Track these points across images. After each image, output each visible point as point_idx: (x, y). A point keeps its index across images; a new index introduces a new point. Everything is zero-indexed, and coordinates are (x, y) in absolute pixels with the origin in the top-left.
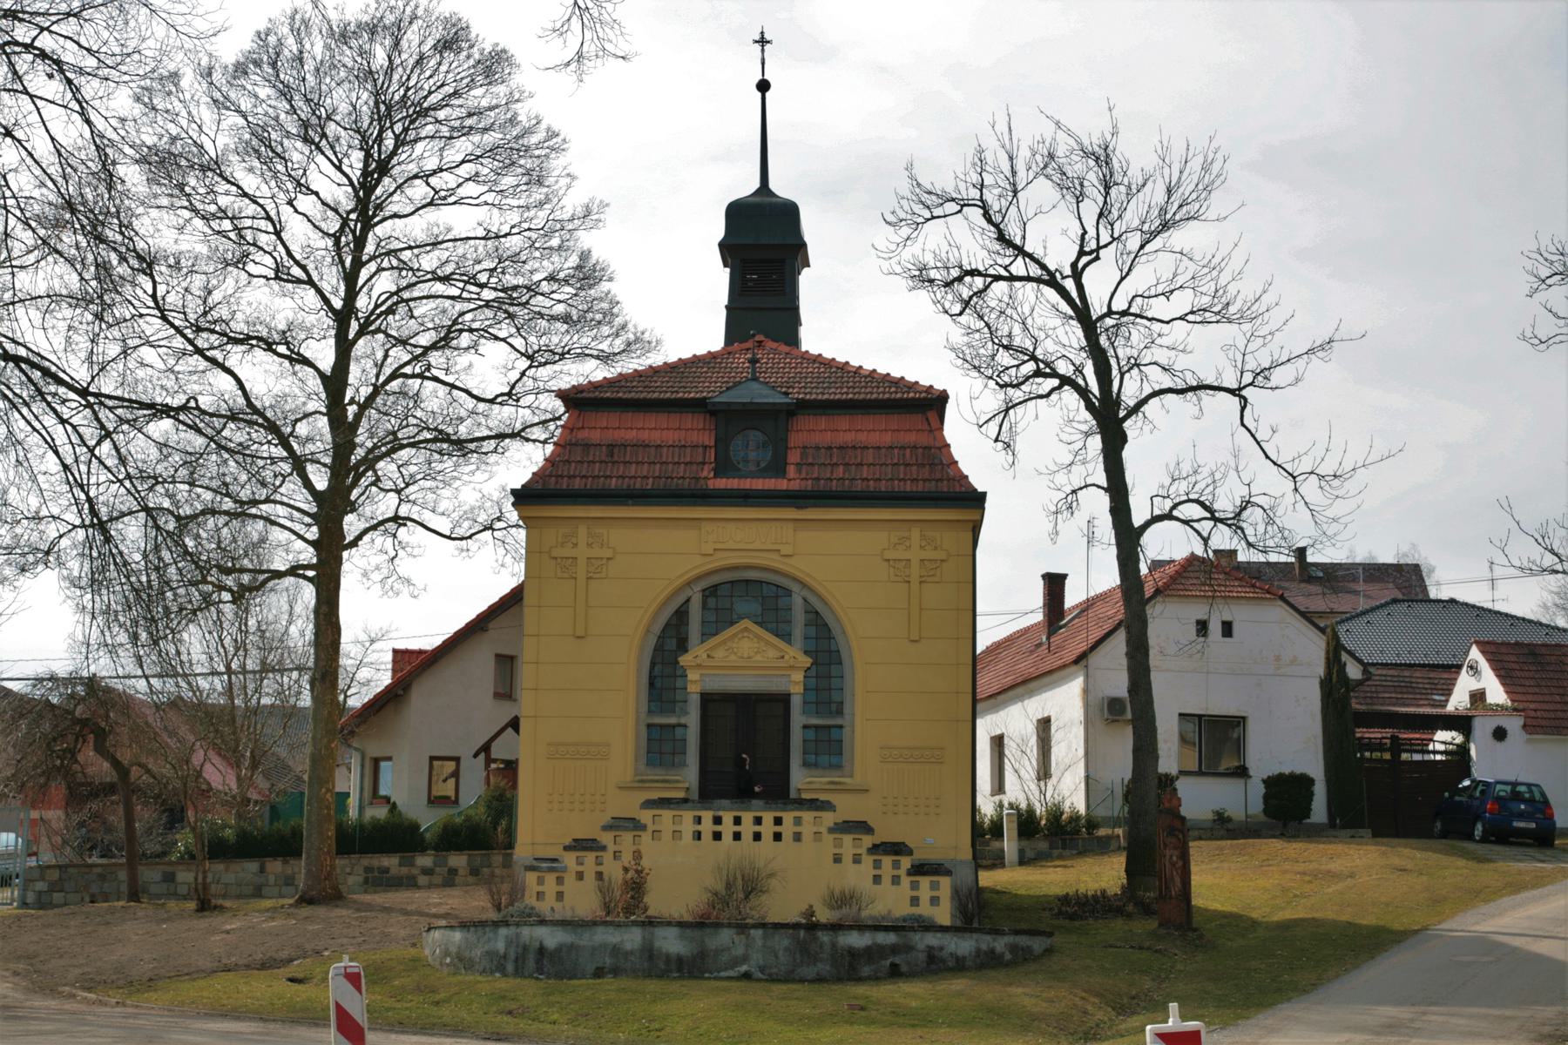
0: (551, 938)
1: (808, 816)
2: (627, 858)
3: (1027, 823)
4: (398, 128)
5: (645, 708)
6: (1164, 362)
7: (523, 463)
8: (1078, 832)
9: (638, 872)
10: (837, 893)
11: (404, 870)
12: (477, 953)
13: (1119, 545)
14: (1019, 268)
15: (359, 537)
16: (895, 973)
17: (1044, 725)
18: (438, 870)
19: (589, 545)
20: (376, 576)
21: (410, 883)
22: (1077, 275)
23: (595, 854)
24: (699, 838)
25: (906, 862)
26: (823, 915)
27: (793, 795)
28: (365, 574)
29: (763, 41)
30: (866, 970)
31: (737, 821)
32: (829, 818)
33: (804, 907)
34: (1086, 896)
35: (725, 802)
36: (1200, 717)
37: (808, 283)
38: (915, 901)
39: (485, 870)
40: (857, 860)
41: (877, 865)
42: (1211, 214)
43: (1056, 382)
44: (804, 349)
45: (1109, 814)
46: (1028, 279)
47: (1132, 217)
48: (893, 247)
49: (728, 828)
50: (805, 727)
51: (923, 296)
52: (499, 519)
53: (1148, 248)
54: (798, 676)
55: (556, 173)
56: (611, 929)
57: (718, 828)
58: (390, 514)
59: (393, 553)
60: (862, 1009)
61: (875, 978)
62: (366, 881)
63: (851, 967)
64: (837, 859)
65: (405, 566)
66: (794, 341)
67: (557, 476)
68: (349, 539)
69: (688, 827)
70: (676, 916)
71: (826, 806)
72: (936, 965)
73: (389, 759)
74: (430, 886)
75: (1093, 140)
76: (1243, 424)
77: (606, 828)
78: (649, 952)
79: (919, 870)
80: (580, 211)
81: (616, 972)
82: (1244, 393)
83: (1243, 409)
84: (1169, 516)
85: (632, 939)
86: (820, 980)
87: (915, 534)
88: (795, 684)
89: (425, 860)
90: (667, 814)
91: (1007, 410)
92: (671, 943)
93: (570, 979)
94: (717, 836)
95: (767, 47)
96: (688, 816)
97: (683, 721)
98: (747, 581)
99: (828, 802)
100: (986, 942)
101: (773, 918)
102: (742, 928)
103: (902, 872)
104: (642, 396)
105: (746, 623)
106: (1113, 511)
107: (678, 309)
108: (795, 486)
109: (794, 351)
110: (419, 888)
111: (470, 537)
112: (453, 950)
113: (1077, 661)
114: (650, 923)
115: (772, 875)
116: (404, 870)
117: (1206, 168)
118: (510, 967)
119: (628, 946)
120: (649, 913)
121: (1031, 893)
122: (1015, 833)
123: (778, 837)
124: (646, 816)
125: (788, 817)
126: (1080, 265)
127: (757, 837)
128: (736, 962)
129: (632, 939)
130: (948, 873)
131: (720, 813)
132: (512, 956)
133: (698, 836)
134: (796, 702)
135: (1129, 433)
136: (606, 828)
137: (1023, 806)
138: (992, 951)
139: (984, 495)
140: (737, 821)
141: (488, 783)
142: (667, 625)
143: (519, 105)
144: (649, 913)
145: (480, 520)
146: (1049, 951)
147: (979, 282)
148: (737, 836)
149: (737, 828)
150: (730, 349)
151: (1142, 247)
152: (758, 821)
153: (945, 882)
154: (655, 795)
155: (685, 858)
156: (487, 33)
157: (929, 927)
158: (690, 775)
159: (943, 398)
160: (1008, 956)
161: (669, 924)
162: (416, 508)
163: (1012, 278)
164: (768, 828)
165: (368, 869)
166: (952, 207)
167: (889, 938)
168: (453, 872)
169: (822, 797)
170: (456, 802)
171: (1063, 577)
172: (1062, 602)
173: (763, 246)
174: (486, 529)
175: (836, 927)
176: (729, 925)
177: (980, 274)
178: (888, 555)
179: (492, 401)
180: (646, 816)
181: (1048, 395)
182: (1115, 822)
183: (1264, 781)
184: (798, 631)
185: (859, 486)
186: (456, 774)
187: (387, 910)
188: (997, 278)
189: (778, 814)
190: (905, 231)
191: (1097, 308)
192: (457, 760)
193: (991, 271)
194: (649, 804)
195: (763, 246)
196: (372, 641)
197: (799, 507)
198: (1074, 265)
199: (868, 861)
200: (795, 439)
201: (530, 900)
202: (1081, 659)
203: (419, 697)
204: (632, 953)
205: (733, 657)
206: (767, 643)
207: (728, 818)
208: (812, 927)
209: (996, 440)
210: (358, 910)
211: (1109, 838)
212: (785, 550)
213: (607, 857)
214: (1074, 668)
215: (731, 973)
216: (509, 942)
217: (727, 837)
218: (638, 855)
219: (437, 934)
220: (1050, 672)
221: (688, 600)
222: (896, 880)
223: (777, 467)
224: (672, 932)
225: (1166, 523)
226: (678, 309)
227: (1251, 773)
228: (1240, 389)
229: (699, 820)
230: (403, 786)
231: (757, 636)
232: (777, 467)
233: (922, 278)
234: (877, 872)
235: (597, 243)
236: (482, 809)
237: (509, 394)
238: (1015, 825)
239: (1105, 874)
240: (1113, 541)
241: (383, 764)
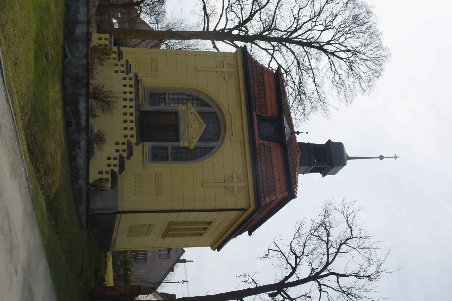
16: (68, 124)
19: (228, 68)
25: (116, 169)
41: (115, 158)
43: (294, 266)
54: (186, 144)
57: (128, 100)
78: (77, 22)
79: (113, 174)
87: (243, 184)
88: (183, 143)
90: (132, 82)
98: (220, 128)
103: (112, 167)
108: (257, 141)
119: (79, 16)
128: (72, 53)
131: (134, 101)
134: (177, 144)
136: (127, 61)
140: (131, 107)
158: (147, 107)
164: (129, 118)
167: (84, 123)
181: (289, 263)
184: (203, 144)
189: (134, 122)
195: (328, 158)
200: (272, 144)
209: (269, 249)
212: (233, 138)
215: (67, 50)
217: (124, 103)
221: (209, 106)
224: (85, 30)
232: (262, 137)
233: (326, 213)
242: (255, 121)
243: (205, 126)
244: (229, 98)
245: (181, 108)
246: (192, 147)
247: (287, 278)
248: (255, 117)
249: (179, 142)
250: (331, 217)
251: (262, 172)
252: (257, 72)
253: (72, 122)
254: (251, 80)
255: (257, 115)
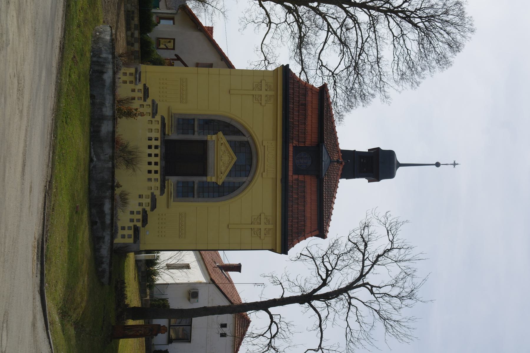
0: (108, 77)
1: (158, 184)
2: (141, 110)
3: (152, 263)
4: (421, 25)
5: (201, 117)
6: (329, 317)
7: (295, 69)
8: (148, 282)
9: (136, 114)
10: (127, 197)
11: (133, 26)
12: (101, 45)
13: (262, 302)
14: (367, 263)
15: (264, 8)
16: (92, 223)
17: (187, 267)
18: (133, 39)
20: (247, 15)
21: (128, 28)
22: (364, 285)
23: (142, 96)
24: (149, 140)
25: (139, 224)
26: (118, 191)
27: (167, 177)
28: (249, 10)
29: (455, 164)
30: (94, 211)
31: (156, 155)
32: (157, 193)
33: (121, 183)
34: (124, 291)
35: (164, 150)
36: (191, 325)
37: (362, 182)
38: (123, 228)
39: (133, 57)
40: (140, 204)
41: (138, 213)
42: (387, 337)
44: (340, 180)
45: (155, 294)
46: (363, 266)
47: (387, 307)
48: (377, 215)
49: (153, 151)
50: (194, 182)
51: (357, 225)
52: (269, 63)
53: (375, 313)
54: (214, 179)
55: (404, 85)
56: (111, 102)
57: (153, 147)
58: (272, 21)
59: (256, 21)
60: (76, 212)
61: (90, 215)
62: (128, 11)
63: (95, 204)
64: (140, 196)
65: (251, 26)
66: (342, 177)
67: (294, 83)
68: (262, 3)
69: (154, 135)
70: (117, 130)
71: (162, 192)
72: (96, 240)
73: (174, 24)
74: (127, 36)
75: (418, 294)
76: (308, 350)
77: (153, 101)
78: (102, 118)
79: (136, 230)
80: (387, 94)
81: (93, 104)
82: (320, 350)
83: (314, 350)
84: (272, 321)
85: (108, 111)
86: (90, 191)
87: (271, 226)
88: (211, 179)
89: (137, 34)
90: (159, 126)
91: (313, 258)
92: (106, 128)
93: (90, 84)
94: (150, 147)
95: (452, 166)
96: (158, 135)
97: (196, 133)
98: (252, 159)
99: (164, 193)
100: (106, 260)
101: (117, 171)
102: (112, 158)
103: (135, 223)
104: (325, 117)
105: (235, 159)
106: (275, 300)
107: (354, 133)
108: (290, 178)
109: (339, 177)
110: (126, 31)
111: (262, 51)
112: (102, 36)
113: (212, 280)
114: (114, 119)
115: (134, 169)
116: (133, 26)
117: (405, 335)
118: (95, 59)
120: (118, 119)
121: (125, 267)
122: (148, 258)
123: (150, 172)
124: (158, 118)
125: (158, 176)
126: (368, 286)
127: (150, 163)
128: (98, 156)
129: (108, 111)
130: (135, 242)
131: (159, 149)
132: (100, 60)
133: (150, 139)
134: (204, 179)
135: (303, 305)
136: (153, 101)
137: (158, 261)
138: (102, 263)
139: (287, 254)
140: (156, 155)
141: (166, 59)
142: (234, 127)
143: (429, 71)
144: (118, 119)
145: (268, 55)
146: (102, 284)
147: (362, 247)
148: (150, 155)
149: (153, 155)
150: (340, 152)
151: (376, 310)
152: (156, 164)
153: (131, 241)
154: (166, 121)
155: (140, 133)
156: (457, 59)
157: (113, 236)
158: (174, 136)
159: (324, 237)
160: (100, 269)
161: (114, 127)
162: (273, 30)
163: (364, 260)
164: (153, 168)
165: (133, 12)
166: (391, 237)
168: (132, 45)
169: (166, 190)
170: (158, 48)
171: (240, 271)
172: (230, 271)
173: (377, 165)
174: (265, 57)
175: (113, 198)
176: (113, 153)
177: (365, 248)
178: (263, 217)
179: (319, 58)
180: (158, 118)
181: (319, 275)
182: (152, 296)
183: (167, 350)
184: (232, 179)
185: (290, 204)
186: (167, 48)
187: (118, 15)
188: (364, 255)
189: (159, 172)
190: (383, 220)
191: (353, 293)
192: (174, 49)
193: (366, 253)
194: (163, 119)
195: (377, 165)
196: (223, 13)
197: (282, 180)
198: (368, 284)
199: (140, 209)
200: (308, 178)
201: (123, 70)
202: (213, 281)
203: (197, 35)
204: (102, 111)
205: (221, 153)
206: (227, 167)
207: (158, 151)
208: (113, 188)
209: (301, 254)
210: (118, 3)
211: (146, 293)
212: (265, 174)
213: (142, 102)
214: (209, 278)
215: (93, 153)
216: (105, 59)
217: (149, 151)
218: (142, 114)
219: (109, 29)
220: (207, 269)
221: (244, 135)
222: (132, 220)
223: (296, 171)
224: (110, 129)
225: (269, 321)
226: (354, 133)
227: (170, 345)
228: (321, 349)
229: (156, 139)
230: (164, 28)
231: (230, 163)
232: (296, 171)
234: (135, 213)
235: (376, 101)
236: (156, 57)
237: (322, 65)
238: (151, 258)
239: (133, 298)
240: (263, 300)
241: (172, 21)
242: (291, 154)
243: (235, 159)
244: (263, 125)
245: (211, 138)
246: (220, 183)
247: (315, 291)
248: (291, 149)
249: (206, 176)
250: (371, 229)
251: (292, 212)
252: (299, 93)
253: (96, 222)
254: (291, 106)
255: (293, 146)
